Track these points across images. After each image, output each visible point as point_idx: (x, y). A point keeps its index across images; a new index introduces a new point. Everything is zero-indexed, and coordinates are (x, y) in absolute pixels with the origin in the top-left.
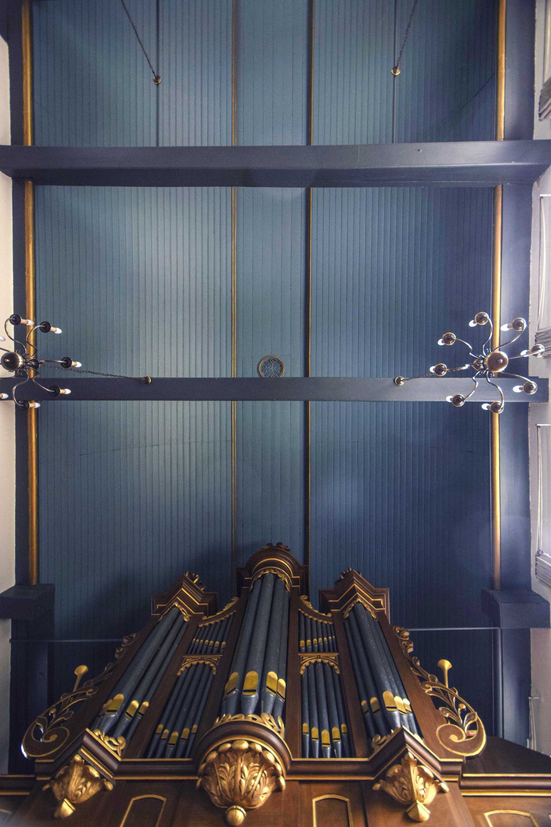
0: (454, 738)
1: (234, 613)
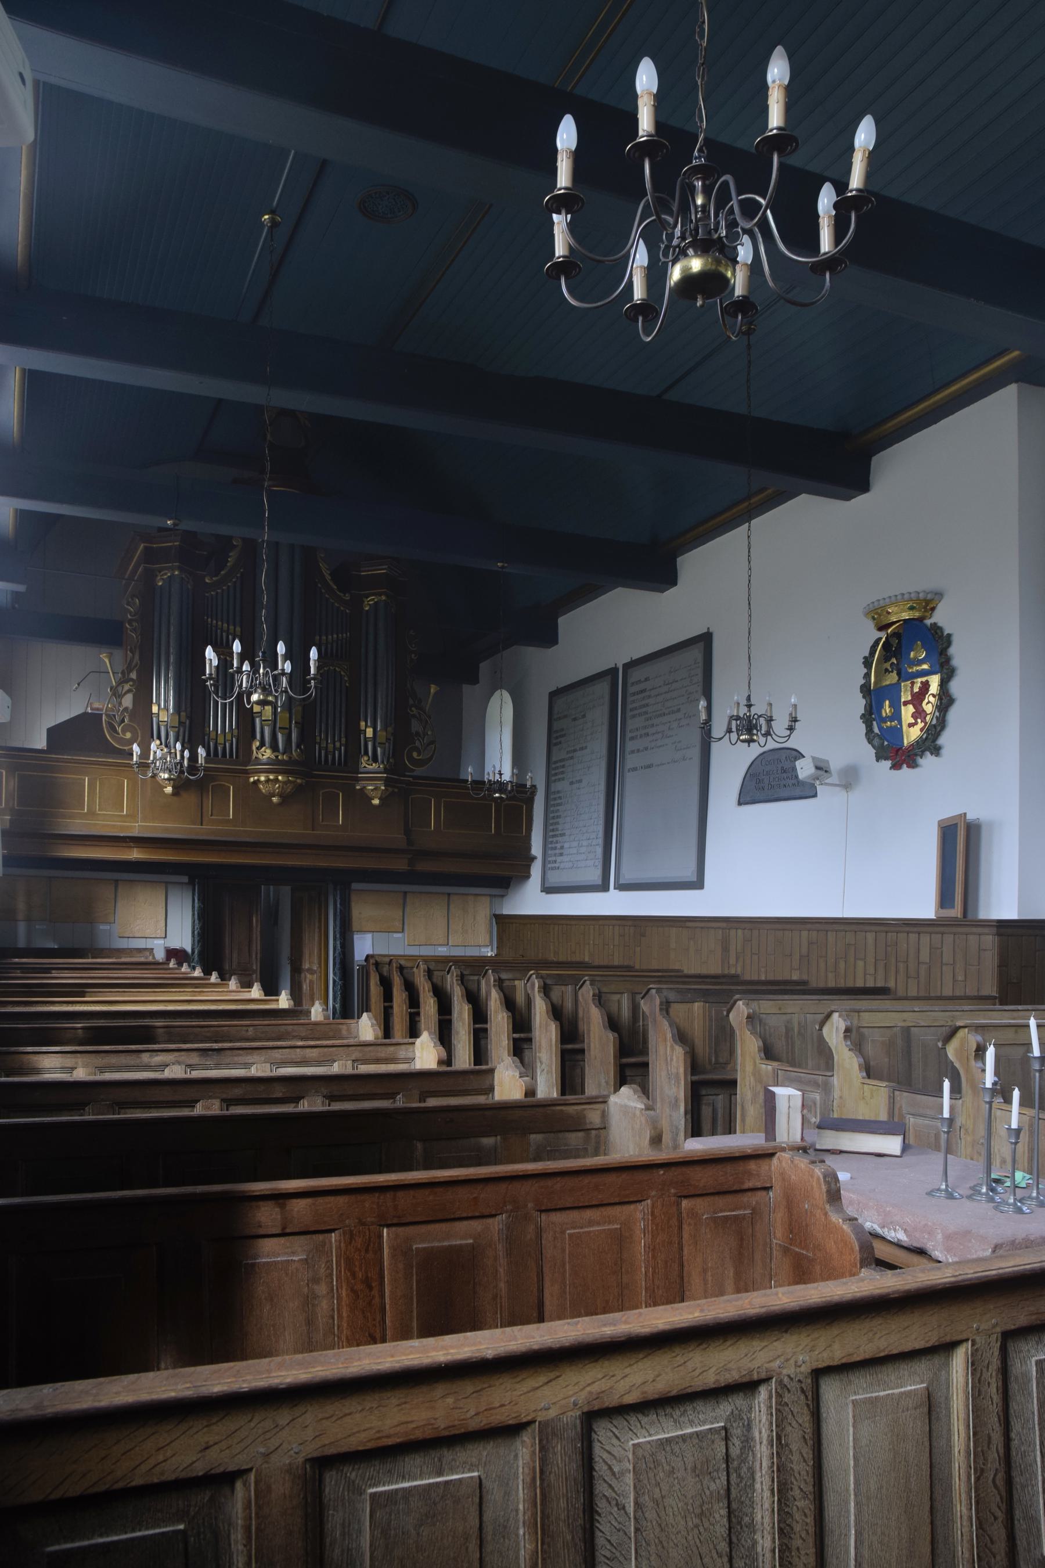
0: (415, 754)
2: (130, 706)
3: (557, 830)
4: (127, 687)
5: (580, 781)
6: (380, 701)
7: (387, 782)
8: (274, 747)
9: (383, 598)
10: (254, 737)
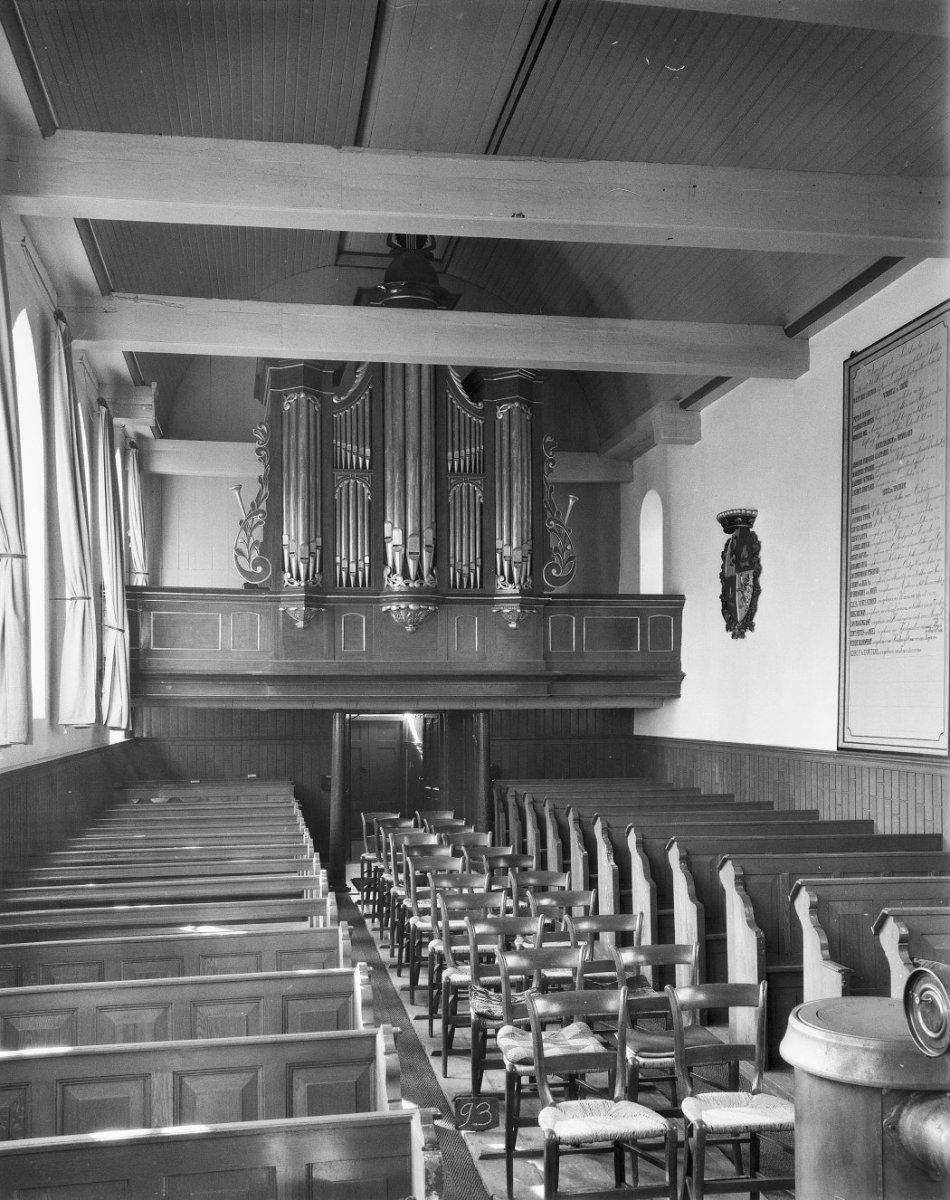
0: (554, 572)
1: (371, 390)
2: (261, 540)
3: (864, 564)
4: (258, 518)
5: (903, 486)
6: (515, 519)
7: (523, 605)
8: (405, 574)
9: (517, 404)
10: (385, 563)
